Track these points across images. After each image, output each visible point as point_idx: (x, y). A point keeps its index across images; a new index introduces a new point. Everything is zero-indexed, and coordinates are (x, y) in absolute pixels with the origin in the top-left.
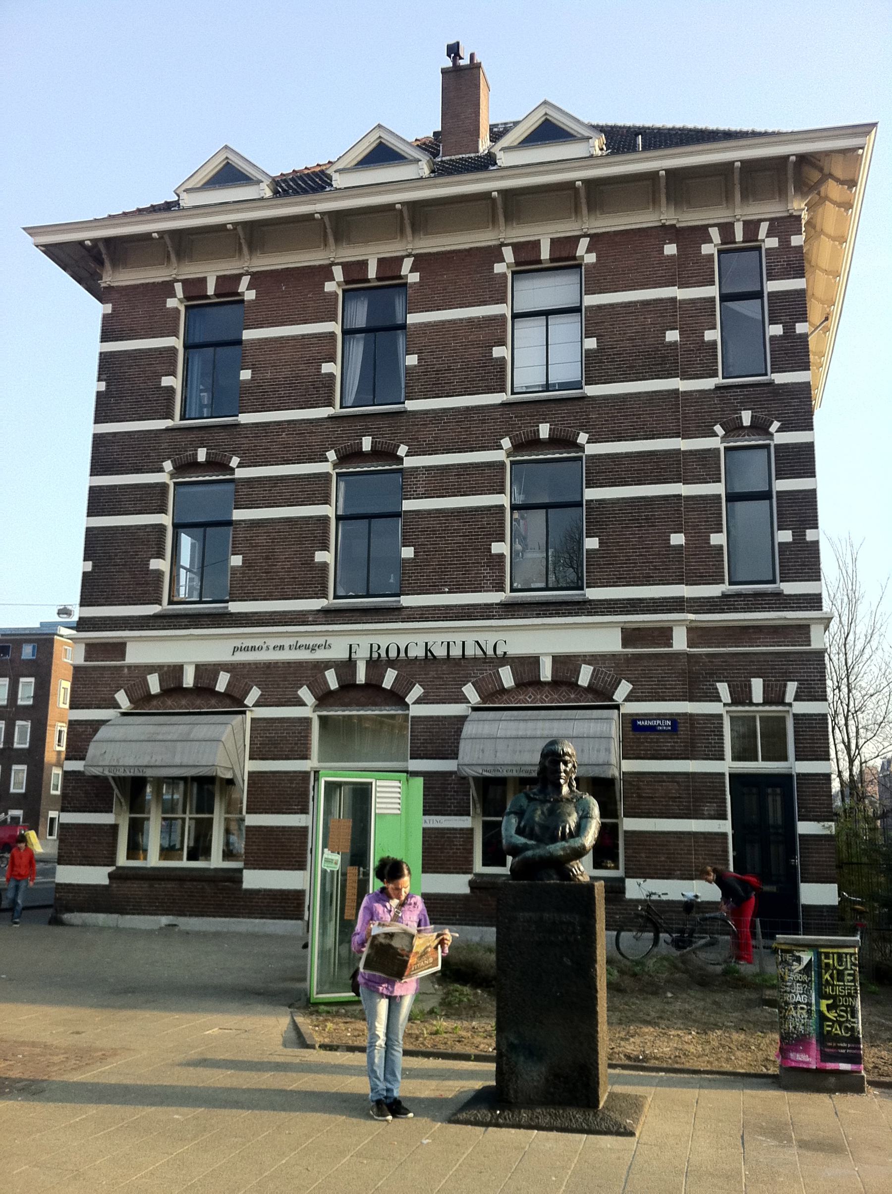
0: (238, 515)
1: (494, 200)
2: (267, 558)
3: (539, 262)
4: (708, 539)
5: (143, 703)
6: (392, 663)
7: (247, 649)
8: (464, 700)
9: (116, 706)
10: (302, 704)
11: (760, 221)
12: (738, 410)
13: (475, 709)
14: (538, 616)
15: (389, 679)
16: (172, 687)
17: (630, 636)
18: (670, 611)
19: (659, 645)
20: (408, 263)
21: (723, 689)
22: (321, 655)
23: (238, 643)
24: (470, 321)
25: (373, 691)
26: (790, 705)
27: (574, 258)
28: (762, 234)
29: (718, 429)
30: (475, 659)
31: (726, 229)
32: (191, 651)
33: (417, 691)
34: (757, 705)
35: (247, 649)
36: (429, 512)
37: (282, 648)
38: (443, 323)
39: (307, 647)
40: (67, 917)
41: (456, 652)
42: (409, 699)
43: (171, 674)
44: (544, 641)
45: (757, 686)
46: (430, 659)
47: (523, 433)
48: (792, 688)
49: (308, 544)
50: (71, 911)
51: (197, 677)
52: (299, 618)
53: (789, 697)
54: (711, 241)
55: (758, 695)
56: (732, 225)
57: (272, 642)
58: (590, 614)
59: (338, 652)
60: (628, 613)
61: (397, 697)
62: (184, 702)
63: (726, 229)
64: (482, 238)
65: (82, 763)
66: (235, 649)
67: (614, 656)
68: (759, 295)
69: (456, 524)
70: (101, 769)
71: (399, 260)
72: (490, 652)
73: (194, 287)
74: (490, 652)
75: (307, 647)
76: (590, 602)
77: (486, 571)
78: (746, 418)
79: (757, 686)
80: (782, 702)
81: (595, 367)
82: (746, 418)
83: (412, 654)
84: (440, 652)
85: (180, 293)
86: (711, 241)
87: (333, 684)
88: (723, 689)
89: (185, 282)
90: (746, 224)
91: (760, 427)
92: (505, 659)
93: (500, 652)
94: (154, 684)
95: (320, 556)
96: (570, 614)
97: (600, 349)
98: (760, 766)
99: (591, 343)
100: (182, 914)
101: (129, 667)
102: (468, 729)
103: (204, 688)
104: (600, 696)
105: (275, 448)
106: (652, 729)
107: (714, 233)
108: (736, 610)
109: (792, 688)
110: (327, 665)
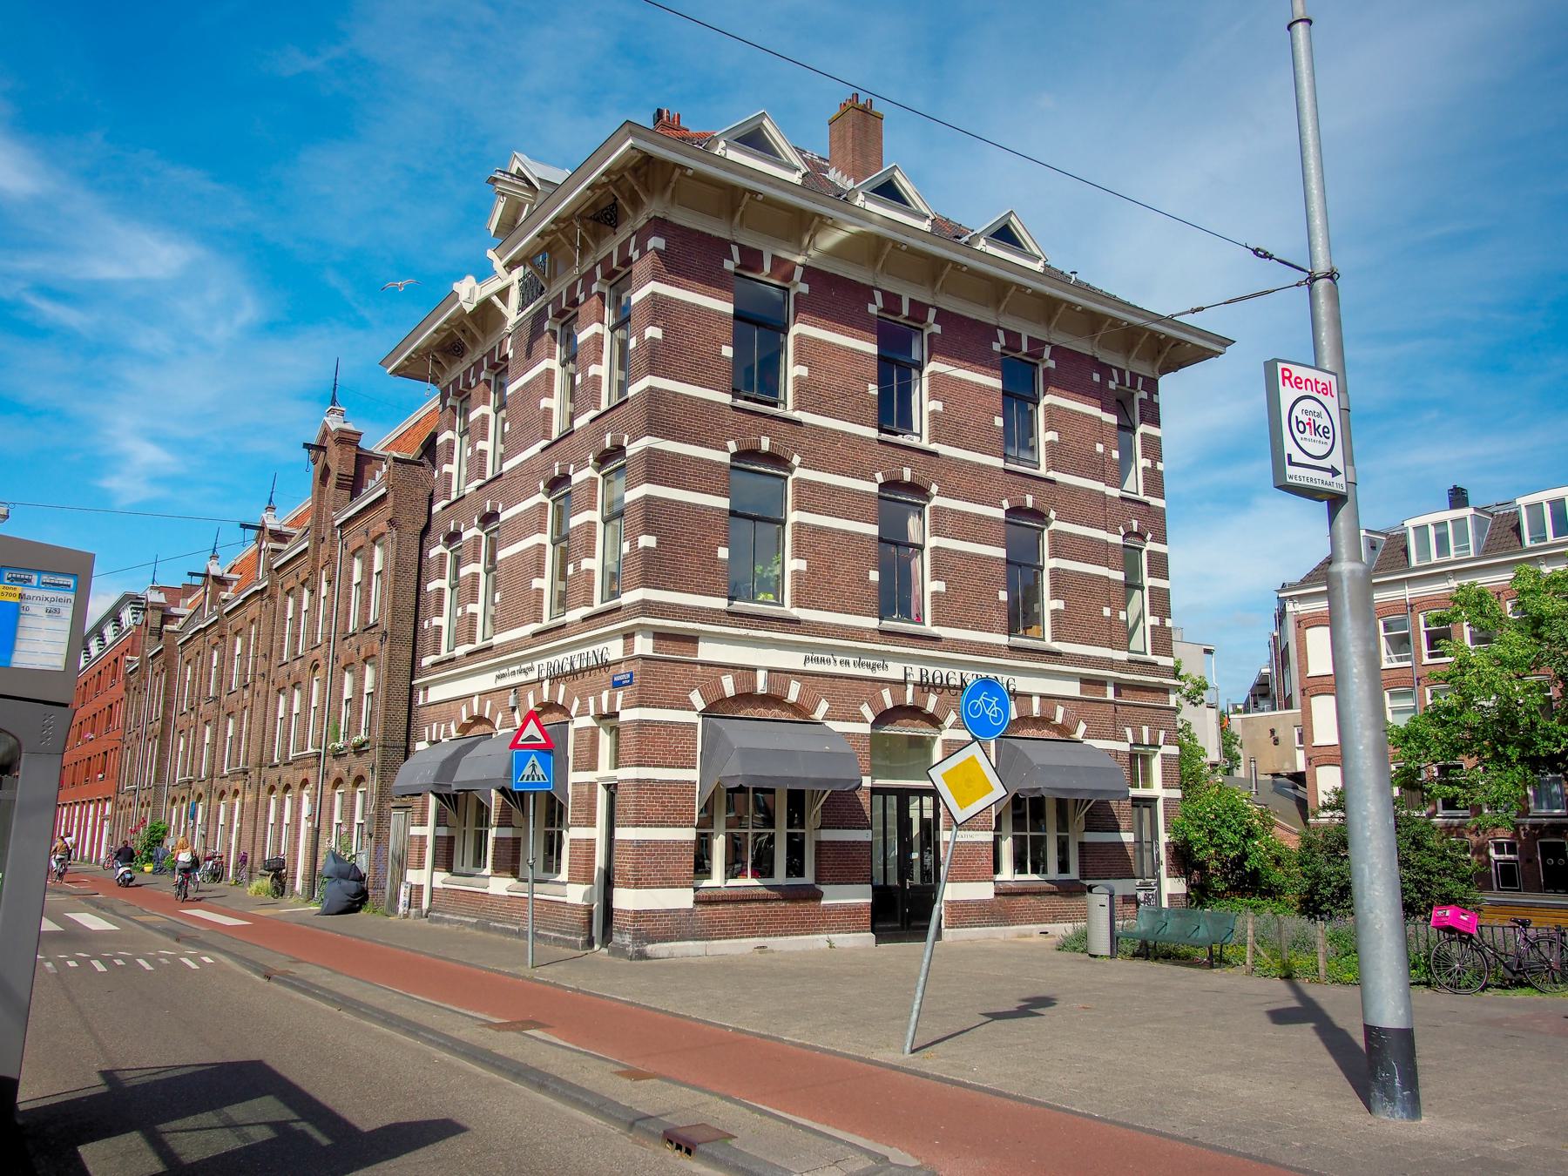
21: (1129, 731)
22: (880, 674)
25: (915, 712)
36: (956, 552)
37: (847, 663)
51: (769, 682)
59: (895, 671)
75: (868, 665)
83: (952, 682)
88: (1129, 731)
91: (1140, 536)
96: (1045, 662)
101: (703, 664)
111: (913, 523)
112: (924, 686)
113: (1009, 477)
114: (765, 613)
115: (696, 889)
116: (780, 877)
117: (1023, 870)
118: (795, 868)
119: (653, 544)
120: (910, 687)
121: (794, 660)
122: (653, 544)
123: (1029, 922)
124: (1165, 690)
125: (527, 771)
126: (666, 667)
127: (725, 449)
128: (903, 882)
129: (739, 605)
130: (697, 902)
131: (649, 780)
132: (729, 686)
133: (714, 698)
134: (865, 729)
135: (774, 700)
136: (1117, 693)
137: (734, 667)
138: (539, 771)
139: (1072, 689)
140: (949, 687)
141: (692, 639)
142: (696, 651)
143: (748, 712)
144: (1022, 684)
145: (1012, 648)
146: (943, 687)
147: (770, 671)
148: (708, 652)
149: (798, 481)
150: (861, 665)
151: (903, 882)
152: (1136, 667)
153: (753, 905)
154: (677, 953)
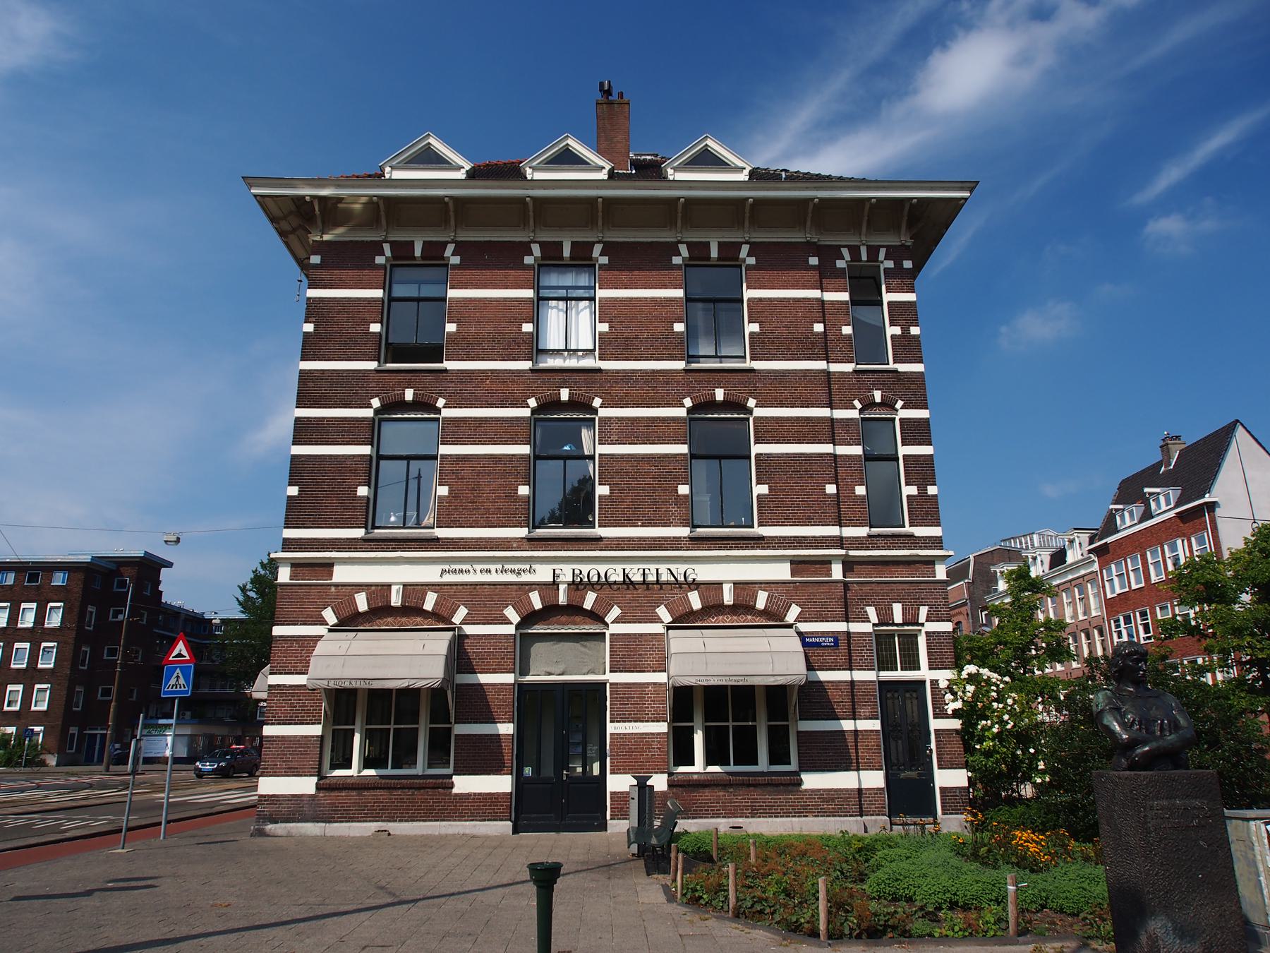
0: (445, 450)
1: (447, 204)
2: (473, 489)
3: (414, 258)
4: (450, 492)
5: (350, 621)
6: (591, 586)
7: (455, 572)
8: (657, 620)
9: (324, 623)
10: (507, 622)
11: (594, 243)
12: (870, 390)
13: (330, 631)
14: (720, 548)
15: (589, 600)
16: (713, 608)
17: (798, 565)
18: (828, 548)
19: (821, 575)
20: (745, 249)
21: (871, 612)
22: (526, 578)
23: (446, 567)
24: (653, 300)
25: (574, 610)
26: (922, 625)
27: (443, 258)
28: (882, 256)
29: (857, 403)
30: (668, 583)
31: (855, 251)
32: (396, 574)
33: (616, 612)
34: (897, 625)
35: (455, 572)
36: (623, 456)
37: (489, 571)
38: (631, 299)
39: (513, 571)
40: (270, 827)
41: (651, 578)
42: (608, 619)
43: (379, 591)
44: (727, 572)
45: (897, 609)
46: (628, 583)
47: (702, 396)
48: (924, 611)
49: (512, 479)
50: (274, 821)
51: (736, 595)
52: (674, 543)
53: (922, 619)
54: (383, 254)
55: (898, 618)
56: (858, 248)
57: (478, 567)
58: (763, 548)
59: (543, 573)
60: (795, 548)
61: (596, 616)
62: (389, 619)
63: (855, 251)
64: (666, 236)
65: (305, 677)
66: (443, 572)
67: (784, 582)
68: (592, 299)
69: (647, 467)
70: (326, 682)
71: (738, 246)
72: (681, 579)
73: (698, 251)
74: (681, 579)
75: (513, 571)
76: (438, 539)
77: (674, 509)
78: (878, 396)
79: (897, 609)
80: (917, 624)
81: (607, 346)
82: (878, 396)
83: (612, 579)
84: (637, 578)
85: (388, 253)
86: (383, 254)
87: (538, 605)
88: (871, 612)
89: (392, 244)
90: (869, 248)
91: (888, 404)
92: (695, 585)
93: (690, 579)
94: (362, 602)
95: (763, 489)
96: (747, 548)
97: (762, 333)
98: (899, 674)
99: (604, 327)
100: (391, 819)
101: (337, 585)
102: (320, 648)
103: (743, 607)
104: (773, 618)
105: (479, 392)
106: (818, 645)
107: (845, 252)
108: (878, 548)
109: (924, 611)
110: (532, 586)
111: (586, 435)
112: (578, 586)
113: (691, 377)
114: (562, 536)
115: (670, 774)
116: (763, 764)
117: (724, 761)
118: (779, 756)
119: (766, 491)
120: (562, 587)
121: (430, 574)
122: (766, 491)
123: (716, 815)
124: (930, 562)
125: (173, 681)
126: (301, 592)
127: (370, 406)
128: (558, 774)
129: (701, 531)
130: (318, 787)
131: (279, 686)
132: (536, 602)
133: (346, 613)
134: (510, 630)
135: (574, 610)
136: (845, 572)
137: (368, 586)
138: (182, 681)
139: (782, 572)
140: (610, 584)
141: (328, 566)
142: (330, 575)
143: (713, 621)
144: (704, 573)
145: (530, 540)
146: (602, 585)
147: (736, 583)
148: (342, 574)
149: (756, 419)
150: (504, 571)
151: (558, 774)
152: (881, 542)
153: (378, 793)
154: (294, 832)
